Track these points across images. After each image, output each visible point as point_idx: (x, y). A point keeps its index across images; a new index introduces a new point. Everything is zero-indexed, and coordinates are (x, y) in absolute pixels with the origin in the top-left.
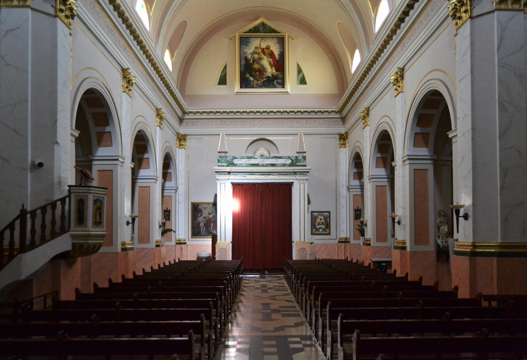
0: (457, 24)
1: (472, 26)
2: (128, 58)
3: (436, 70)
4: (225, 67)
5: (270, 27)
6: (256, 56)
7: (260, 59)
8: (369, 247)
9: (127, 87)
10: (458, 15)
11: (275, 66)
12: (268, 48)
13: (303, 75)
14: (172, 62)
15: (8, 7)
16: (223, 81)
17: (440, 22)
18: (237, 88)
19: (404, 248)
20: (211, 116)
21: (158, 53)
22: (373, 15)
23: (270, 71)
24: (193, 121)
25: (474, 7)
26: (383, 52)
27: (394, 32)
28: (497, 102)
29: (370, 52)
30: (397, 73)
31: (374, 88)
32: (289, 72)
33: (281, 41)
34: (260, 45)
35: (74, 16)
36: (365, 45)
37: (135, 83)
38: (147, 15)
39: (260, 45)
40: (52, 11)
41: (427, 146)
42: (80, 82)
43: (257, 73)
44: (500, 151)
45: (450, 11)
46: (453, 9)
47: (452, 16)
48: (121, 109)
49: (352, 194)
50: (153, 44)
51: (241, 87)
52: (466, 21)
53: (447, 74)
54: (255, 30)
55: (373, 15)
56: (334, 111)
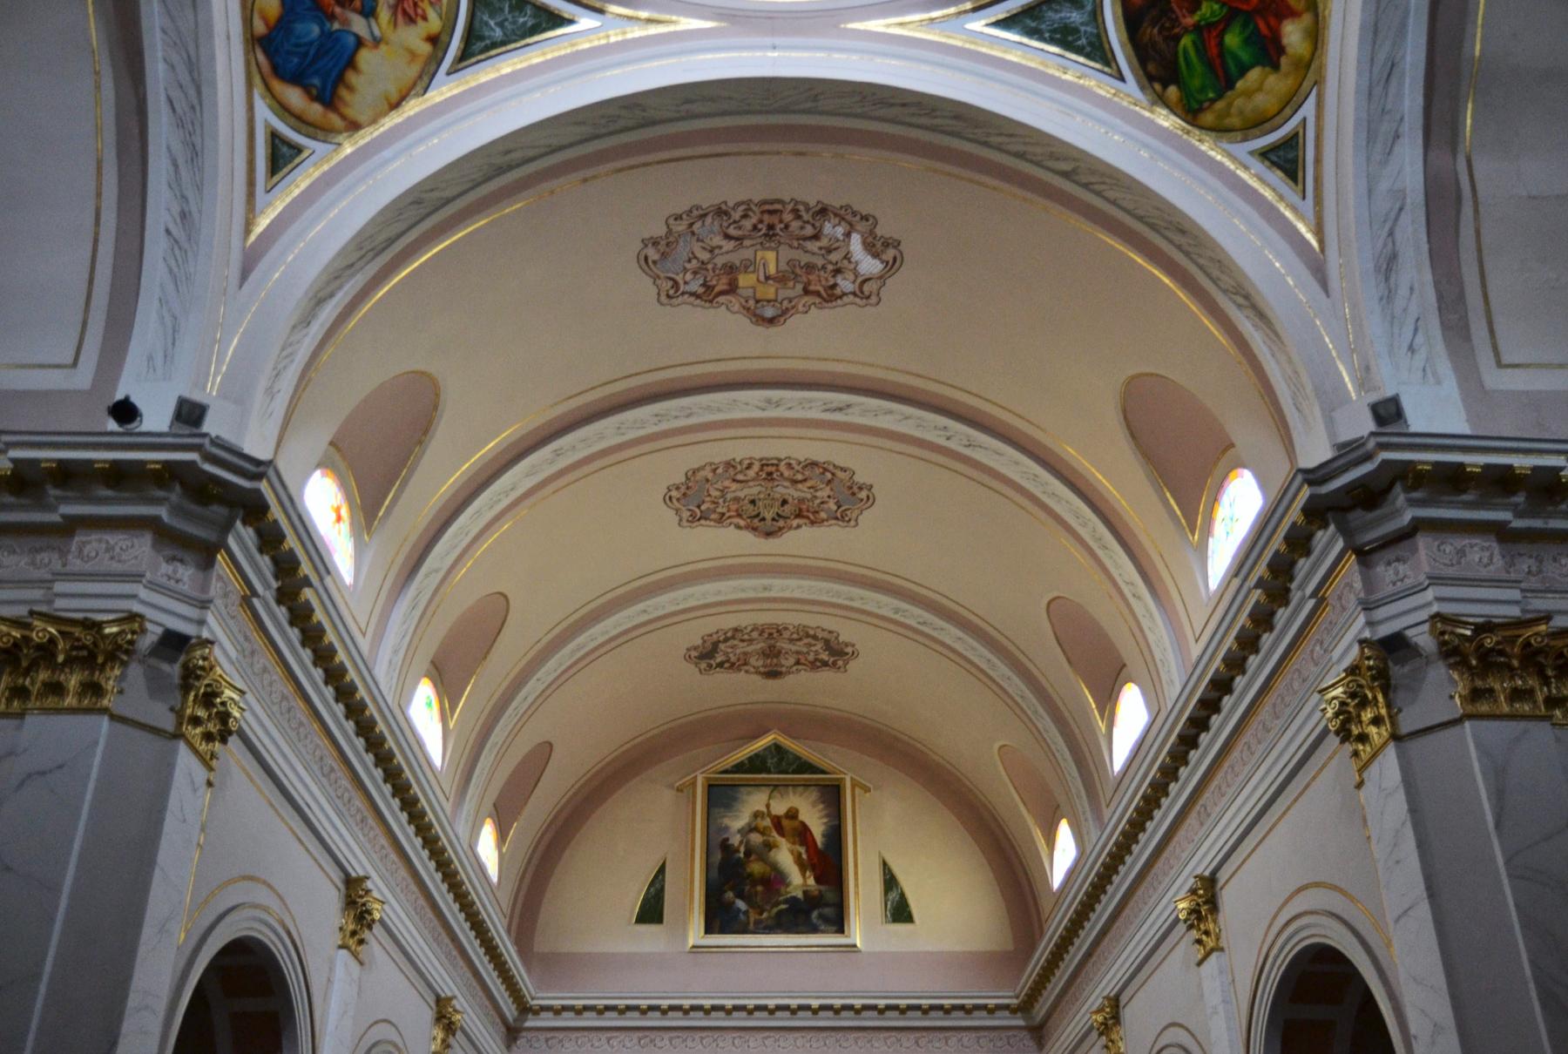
0: (1356, 754)
1: (1402, 757)
2: (368, 846)
3: (1317, 885)
4: (662, 870)
5: (799, 758)
6: (756, 838)
7: (769, 846)
9: (354, 933)
10: (1355, 731)
11: (813, 868)
12: (792, 814)
13: (902, 895)
14: (501, 857)
15: (46, 711)
16: (651, 912)
17: (1260, 805)
18: (695, 933)
20: (611, 1020)
21: (460, 834)
22: (1102, 726)
23: (798, 881)
24: (549, 1035)
25: (1400, 710)
26: (1217, 710)
27: (1169, 773)
28: (1532, 986)
29: (1103, 827)
30: (1193, 892)
31: (1132, 928)
32: (856, 885)
33: (832, 796)
34: (768, 806)
35: (230, 733)
36: (1087, 808)
37: (381, 921)
38: (439, 727)
39: (768, 806)
40: (168, 722)
42: (211, 918)
43: (759, 888)
45: (1330, 720)
46: (1337, 715)
47: (1337, 733)
48: (326, 998)
50: (448, 807)
51: (709, 930)
52: (1385, 744)
53: (1352, 899)
54: (755, 764)
55: (1102, 726)
56: (1006, 1007)
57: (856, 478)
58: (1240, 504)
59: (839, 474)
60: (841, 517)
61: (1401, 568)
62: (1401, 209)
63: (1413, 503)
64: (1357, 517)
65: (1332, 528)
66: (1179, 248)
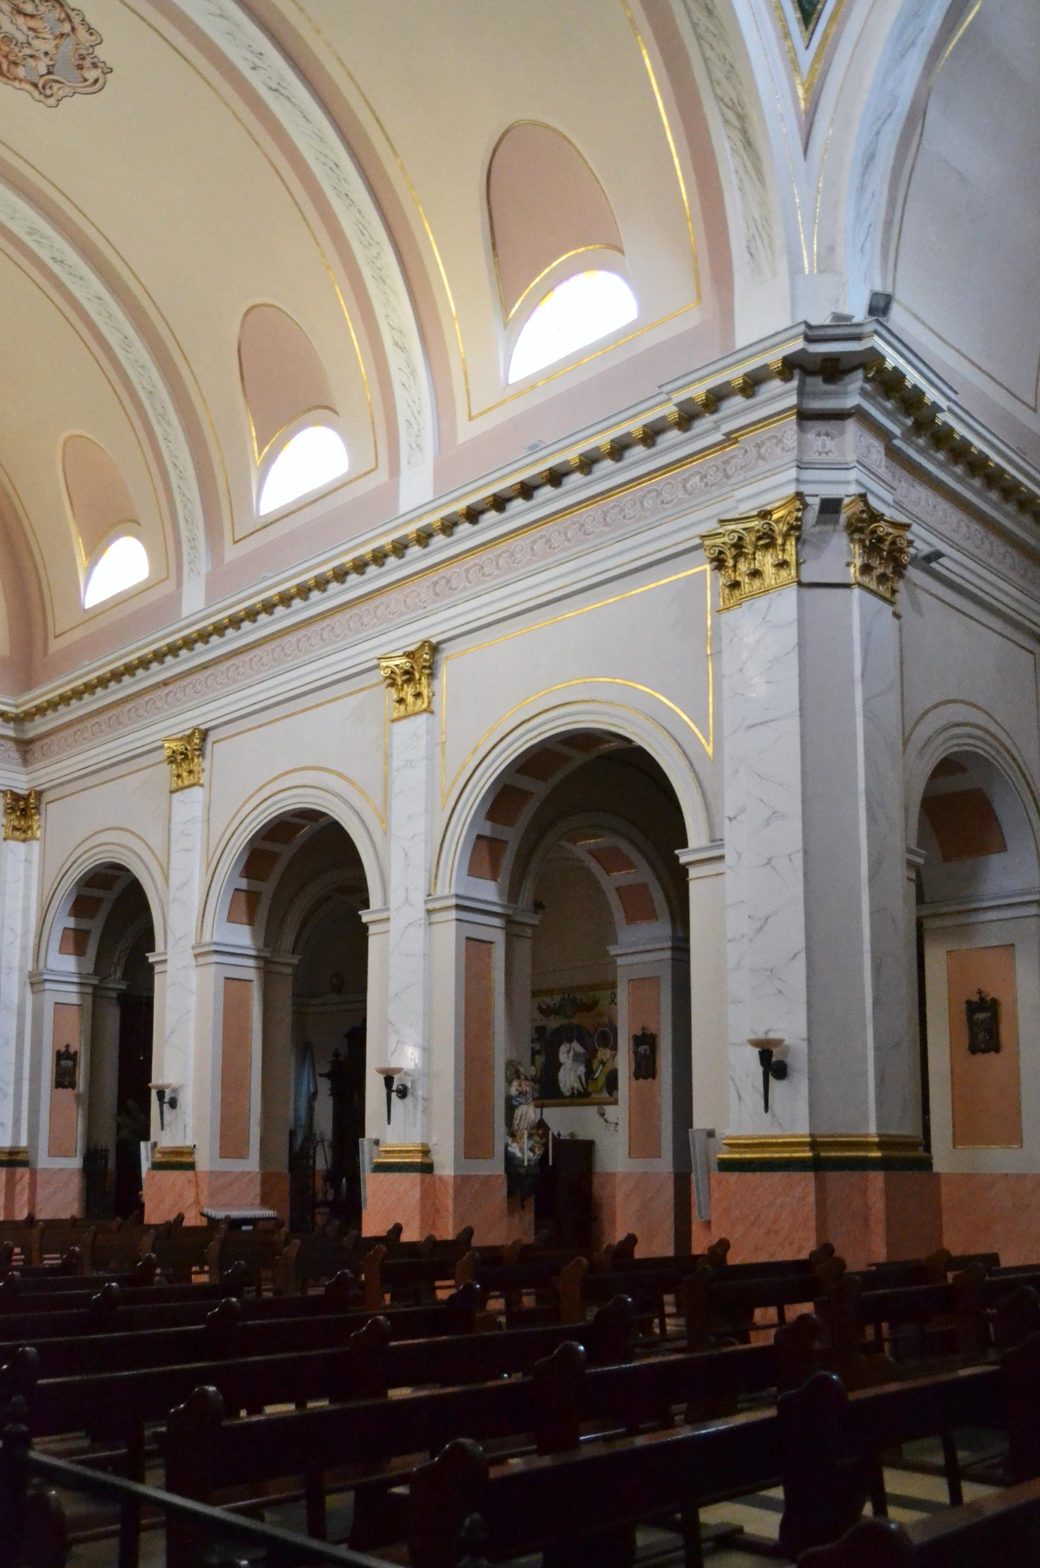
8: (190, 1174)
19: (427, 1168)
25: (804, 562)
41: (494, 878)
44: (872, 914)
49: (49, 1000)
57: (99, 51)
58: (584, 313)
59: (82, 33)
60: (42, 87)
61: (829, 443)
62: (890, 115)
63: (864, 393)
64: (816, 383)
65: (794, 383)
66: (695, 26)
